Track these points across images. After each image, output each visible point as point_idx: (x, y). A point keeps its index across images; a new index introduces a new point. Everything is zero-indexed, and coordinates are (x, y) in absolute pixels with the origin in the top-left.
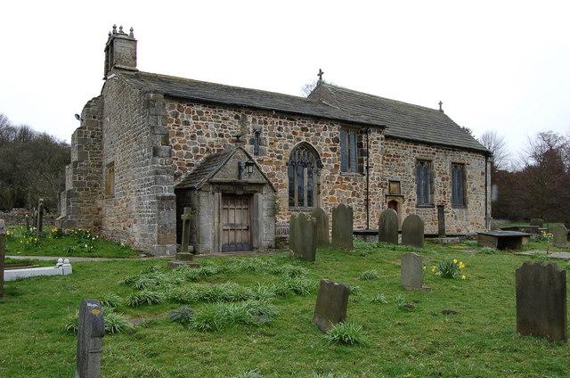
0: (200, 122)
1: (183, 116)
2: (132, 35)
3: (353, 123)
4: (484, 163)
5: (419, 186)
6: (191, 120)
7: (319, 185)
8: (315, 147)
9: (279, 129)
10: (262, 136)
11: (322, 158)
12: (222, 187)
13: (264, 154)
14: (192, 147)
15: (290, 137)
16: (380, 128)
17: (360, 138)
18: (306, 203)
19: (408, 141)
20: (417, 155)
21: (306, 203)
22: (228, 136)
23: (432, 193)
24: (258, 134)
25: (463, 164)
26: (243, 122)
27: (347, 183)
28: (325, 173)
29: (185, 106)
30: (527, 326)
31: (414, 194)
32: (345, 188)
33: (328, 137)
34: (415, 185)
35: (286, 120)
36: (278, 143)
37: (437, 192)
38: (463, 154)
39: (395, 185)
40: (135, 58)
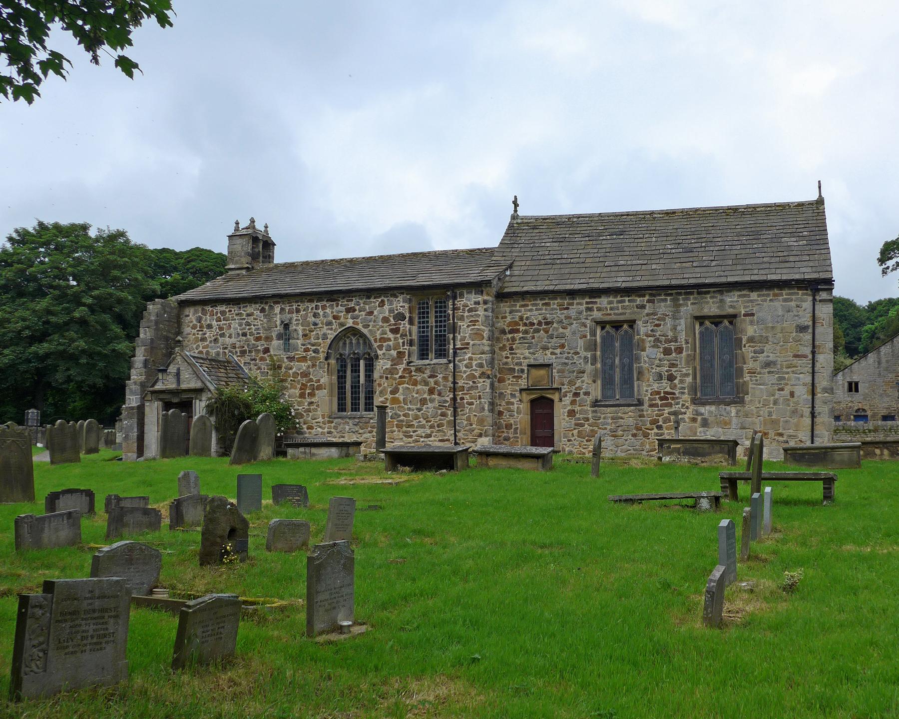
0: (223, 322)
2: (266, 231)
6: (214, 323)
10: (293, 327)
11: (375, 345)
12: (162, 396)
15: (329, 324)
18: (362, 406)
19: (572, 294)
21: (362, 406)
22: (251, 334)
24: (286, 326)
26: (269, 317)
28: (382, 365)
29: (209, 308)
33: (387, 314)
35: (325, 303)
36: (314, 333)
39: (542, 372)
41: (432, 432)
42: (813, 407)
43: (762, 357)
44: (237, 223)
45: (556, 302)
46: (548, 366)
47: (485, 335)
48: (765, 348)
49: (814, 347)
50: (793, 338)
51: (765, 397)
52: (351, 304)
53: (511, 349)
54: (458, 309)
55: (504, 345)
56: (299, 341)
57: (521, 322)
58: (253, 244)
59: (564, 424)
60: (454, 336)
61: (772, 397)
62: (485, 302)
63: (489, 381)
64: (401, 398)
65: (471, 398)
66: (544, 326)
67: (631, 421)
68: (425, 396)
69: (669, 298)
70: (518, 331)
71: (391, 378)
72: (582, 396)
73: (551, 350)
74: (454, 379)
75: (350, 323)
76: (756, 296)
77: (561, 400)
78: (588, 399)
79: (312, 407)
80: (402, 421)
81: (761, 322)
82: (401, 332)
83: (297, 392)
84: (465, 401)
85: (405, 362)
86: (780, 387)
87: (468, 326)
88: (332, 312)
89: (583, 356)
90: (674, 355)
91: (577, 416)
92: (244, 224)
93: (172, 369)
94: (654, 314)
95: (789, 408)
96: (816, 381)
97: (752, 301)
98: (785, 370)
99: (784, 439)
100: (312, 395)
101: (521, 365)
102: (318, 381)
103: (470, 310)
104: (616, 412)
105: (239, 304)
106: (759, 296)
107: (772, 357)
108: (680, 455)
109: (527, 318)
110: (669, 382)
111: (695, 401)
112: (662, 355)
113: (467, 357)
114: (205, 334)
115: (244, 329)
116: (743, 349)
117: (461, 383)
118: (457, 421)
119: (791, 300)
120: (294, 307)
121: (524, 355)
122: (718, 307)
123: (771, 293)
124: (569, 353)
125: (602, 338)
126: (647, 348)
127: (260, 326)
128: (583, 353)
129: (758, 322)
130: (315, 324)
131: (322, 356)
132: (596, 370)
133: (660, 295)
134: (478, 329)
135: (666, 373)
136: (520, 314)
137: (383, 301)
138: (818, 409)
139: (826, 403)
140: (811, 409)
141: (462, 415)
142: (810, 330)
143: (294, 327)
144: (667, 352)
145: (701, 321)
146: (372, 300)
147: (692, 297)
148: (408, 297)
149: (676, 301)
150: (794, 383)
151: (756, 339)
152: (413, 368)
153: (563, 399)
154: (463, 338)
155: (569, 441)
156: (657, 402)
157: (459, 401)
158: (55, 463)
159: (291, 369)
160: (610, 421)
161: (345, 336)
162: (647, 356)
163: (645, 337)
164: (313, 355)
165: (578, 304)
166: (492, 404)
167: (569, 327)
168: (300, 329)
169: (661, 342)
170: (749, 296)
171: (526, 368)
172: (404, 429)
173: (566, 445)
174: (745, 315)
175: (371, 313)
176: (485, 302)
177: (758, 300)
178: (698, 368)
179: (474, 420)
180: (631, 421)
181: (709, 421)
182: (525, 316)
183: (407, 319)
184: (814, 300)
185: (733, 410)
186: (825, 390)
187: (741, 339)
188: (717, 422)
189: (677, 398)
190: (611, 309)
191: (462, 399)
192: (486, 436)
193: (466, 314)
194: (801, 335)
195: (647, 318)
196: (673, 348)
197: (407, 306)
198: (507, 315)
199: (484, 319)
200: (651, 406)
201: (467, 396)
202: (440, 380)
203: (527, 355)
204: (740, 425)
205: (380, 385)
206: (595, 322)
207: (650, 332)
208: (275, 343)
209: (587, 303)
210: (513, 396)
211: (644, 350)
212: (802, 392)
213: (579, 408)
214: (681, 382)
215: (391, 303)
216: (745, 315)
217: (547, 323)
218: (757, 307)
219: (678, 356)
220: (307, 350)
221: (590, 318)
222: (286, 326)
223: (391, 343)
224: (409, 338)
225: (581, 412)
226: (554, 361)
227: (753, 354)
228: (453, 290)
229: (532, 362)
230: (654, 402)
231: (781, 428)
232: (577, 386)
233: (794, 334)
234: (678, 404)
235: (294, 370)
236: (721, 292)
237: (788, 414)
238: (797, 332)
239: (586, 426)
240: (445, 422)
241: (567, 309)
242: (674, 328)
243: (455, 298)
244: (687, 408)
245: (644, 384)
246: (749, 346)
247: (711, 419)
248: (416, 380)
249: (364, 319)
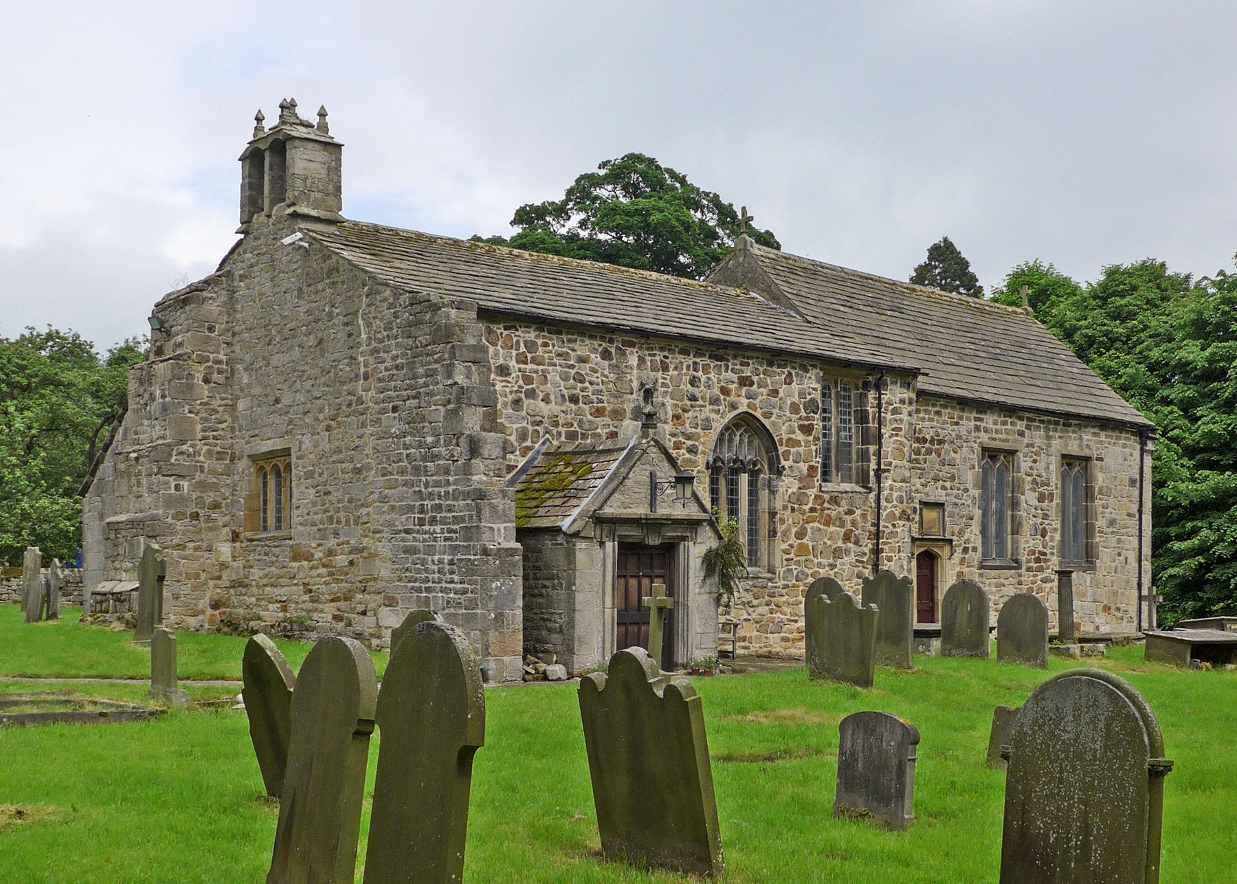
0: (530, 366)
1: (497, 354)
2: (323, 127)
3: (848, 364)
4: (1137, 453)
5: (985, 515)
6: (513, 363)
7: (773, 514)
8: (766, 422)
11: (781, 449)
12: (623, 531)
14: (515, 426)
15: (715, 401)
16: (907, 376)
17: (862, 398)
19: (964, 403)
20: (984, 438)
23: (1016, 531)
24: (648, 394)
25: (1087, 459)
28: (788, 486)
29: (499, 329)
30: (1062, 455)
31: (973, 535)
33: (796, 399)
34: (977, 513)
35: (706, 360)
36: (690, 414)
37: (1026, 530)
38: (1087, 436)
40: (338, 189)
52: (747, 372)
88: (719, 381)
126: (1026, 491)
130: (693, 398)
137: (790, 374)
164: (688, 456)
175: (774, 393)
211: (1023, 494)
217: (941, 442)
223: (801, 449)
241: (957, 424)
248: (829, 516)
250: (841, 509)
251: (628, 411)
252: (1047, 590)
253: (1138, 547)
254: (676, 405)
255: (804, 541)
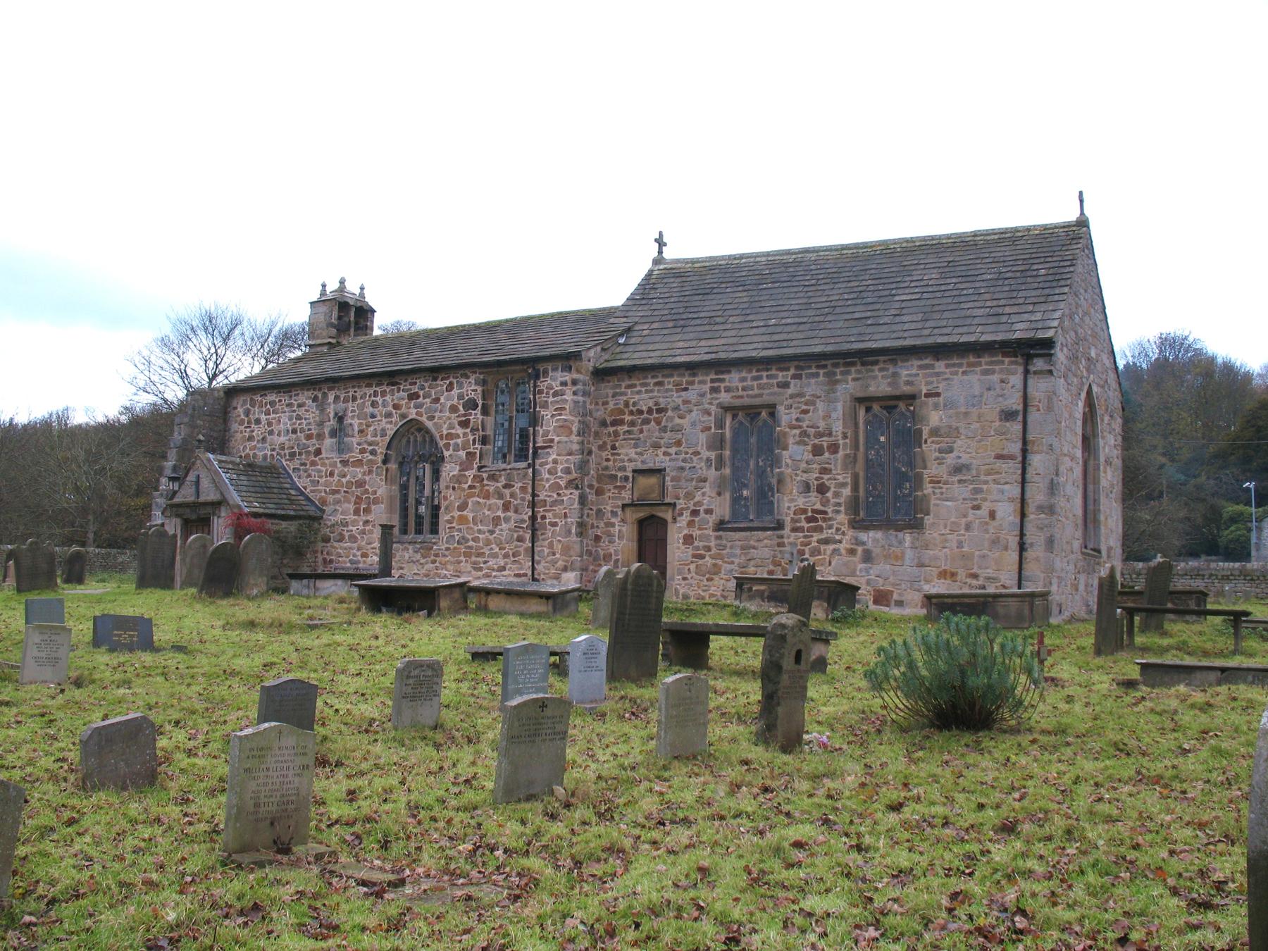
0: (273, 416)
2: (362, 295)
6: (263, 417)
9: (374, 404)
10: (348, 421)
11: (441, 443)
12: (181, 511)
13: (350, 450)
15: (389, 415)
19: (692, 367)
22: (302, 431)
24: (340, 419)
26: (322, 407)
27: (491, 487)
28: (449, 470)
29: (258, 398)
32: (487, 496)
35: (384, 387)
39: (652, 480)
41: (506, 564)
42: (1022, 535)
43: (950, 459)
44: (324, 286)
45: (672, 380)
46: (660, 471)
47: (575, 429)
48: (955, 445)
49: (1025, 442)
50: (995, 430)
51: (953, 519)
52: (415, 389)
53: (614, 448)
54: (541, 392)
55: (605, 443)
56: (353, 439)
57: (626, 410)
58: (339, 312)
59: (678, 554)
60: (534, 430)
61: (964, 520)
62: (574, 382)
63: (577, 493)
64: (470, 516)
65: (555, 516)
66: (655, 415)
67: (766, 553)
68: (499, 513)
69: (821, 372)
70: (621, 422)
71: (459, 488)
72: (702, 514)
73: (663, 449)
74: (533, 489)
75: (413, 414)
76: (943, 366)
77: (674, 519)
78: (711, 520)
79: (367, 528)
80: (471, 548)
81: (949, 405)
82: (471, 425)
83: (351, 507)
84: (547, 521)
85: (475, 466)
86: (975, 503)
87: (553, 416)
88: (393, 400)
89: (705, 457)
90: (827, 455)
91: (696, 543)
92: (332, 286)
93: (191, 477)
94: (801, 395)
95: (987, 536)
96: (1028, 495)
97: (937, 374)
98: (983, 478)
99: (980, 583)
100: (367, 511)
101: (625, 470)
102: (375, 492)
103: (556, 394)
104: (746, 539)
105: (290, 391)
106: (947, 366)
107: (965, 459)
108: (763, 601)
109: (634, 404)
110: (820, 496)
111: (856, 524)
112: (811, 456)
113: (550, 459)
114: (253, 431)
115: (295, 424)
116: (924, 446)
117: (542, 495)
118: (536, 549)
119: (993, 372)
120: (350, 394)
121: (630, 456)
122: (889, 384)
123: (964, 361)
124: (687, 453)
125: (733, 429)
126: (790, 446)
127: (312, 420)
128: (706, 454)
129: (945, 405)
130: (373, 416)
131: (380, 458)
132: (722, 477)
133: (810, 367)
134: (565, 420)
135: (816, 483)
136: (625, 398)
137: (451, 384)
138: (1028, 539)
139: (1042, 529)
140: (1018, 538)
141: (543, 540)
142: (1020, 418)
143: (350, 421)
144: (817, 451)
145: (868, 404)
146: (439, 382)
147: (853, 369)
148: (482, 377)
149: (830, 375)
150: (996, 498)
151: (942, 431)
152: (485, 475)
153: (678, 519)
154: (546, 433)
155: (685, 579)
156: (802, 524)
157: (539, 520)
158: (24, 591)
159: (344, 476)
160: (738, 551)
161: (408, 431)
162: (790, 457)
163: (787, 430)
164: (371, 457)
165: (700, 382)
166: (581, 525)
167: (688, 416)
168: (356, 422)
169: (808, 436)
170: (932, 366)
171: (630, 475)
172: (474, 559)
173: (680, 585)
174: (927, 395)
175: (437, 400)
176: (574, 382)
177: (945, 373)
178: (862, 474)
179: (558, 547)
180: (766, 553)
181: (874, 555)
182: (632, 401)
183: (479, 408)
184: (1026, 372)
185: (908, 538)
186: (1040, 509)
187: (920, 432)
188: (885, 556)
189: (830, 519)
190: (744, 389)
191: (544, 517)
192: (573, 570)
193: (551, 399)
194: (1008, 424)
195: (790, 401)
196: (825, 444)
197: (479, 389)
198: (609, 399)
199: (572, 405)
200: (794, 530)
201: (550, 514)
202: (518, 491)
203: (634, 456)
204: (916, 561)
205: (446, 498)
206: (722, 408)
207: (794, 422)
208: (329, 442)
209: (713, 381)
210: (614, 514)
211: (785, 448)
212: (1007, 512)
213: (699, 532)
214: (836, 495)
215: (461, 387)
216: (927, 395)
217: (660, 411)
218: (944, 383)
219: (832, 457)
220: (363, 451)
221: (716, 402)
222: (340, 419)
223: (459, 441)
224: (481, 433)
225: (701, 538)
226: (668, 464)
227: (937, 454)
228: (532, 367)
229: (640, 466)
230: (798, 525)
231: (976, 567)
232: (696, 500)
233: (997, 424)
234: (830, 527)
235: (348, 477)
236: (894, 362)
237: (986, 544)
238: (1001, 420)
239: (707, 558)
240: (521, 549)
241: (686, 389)
242: (827, 416)
243: (537, 377)
244: (843, 533)
245: (785, 499)
246: (933, 442)
247: (876, 551)
248: (487, 491)
249: (429, 408)
250: (499, 485)
251: (327, 433)
252: (829, 552)
253: (1019, 496)
254: (361, 424)
255: (465, 513)
